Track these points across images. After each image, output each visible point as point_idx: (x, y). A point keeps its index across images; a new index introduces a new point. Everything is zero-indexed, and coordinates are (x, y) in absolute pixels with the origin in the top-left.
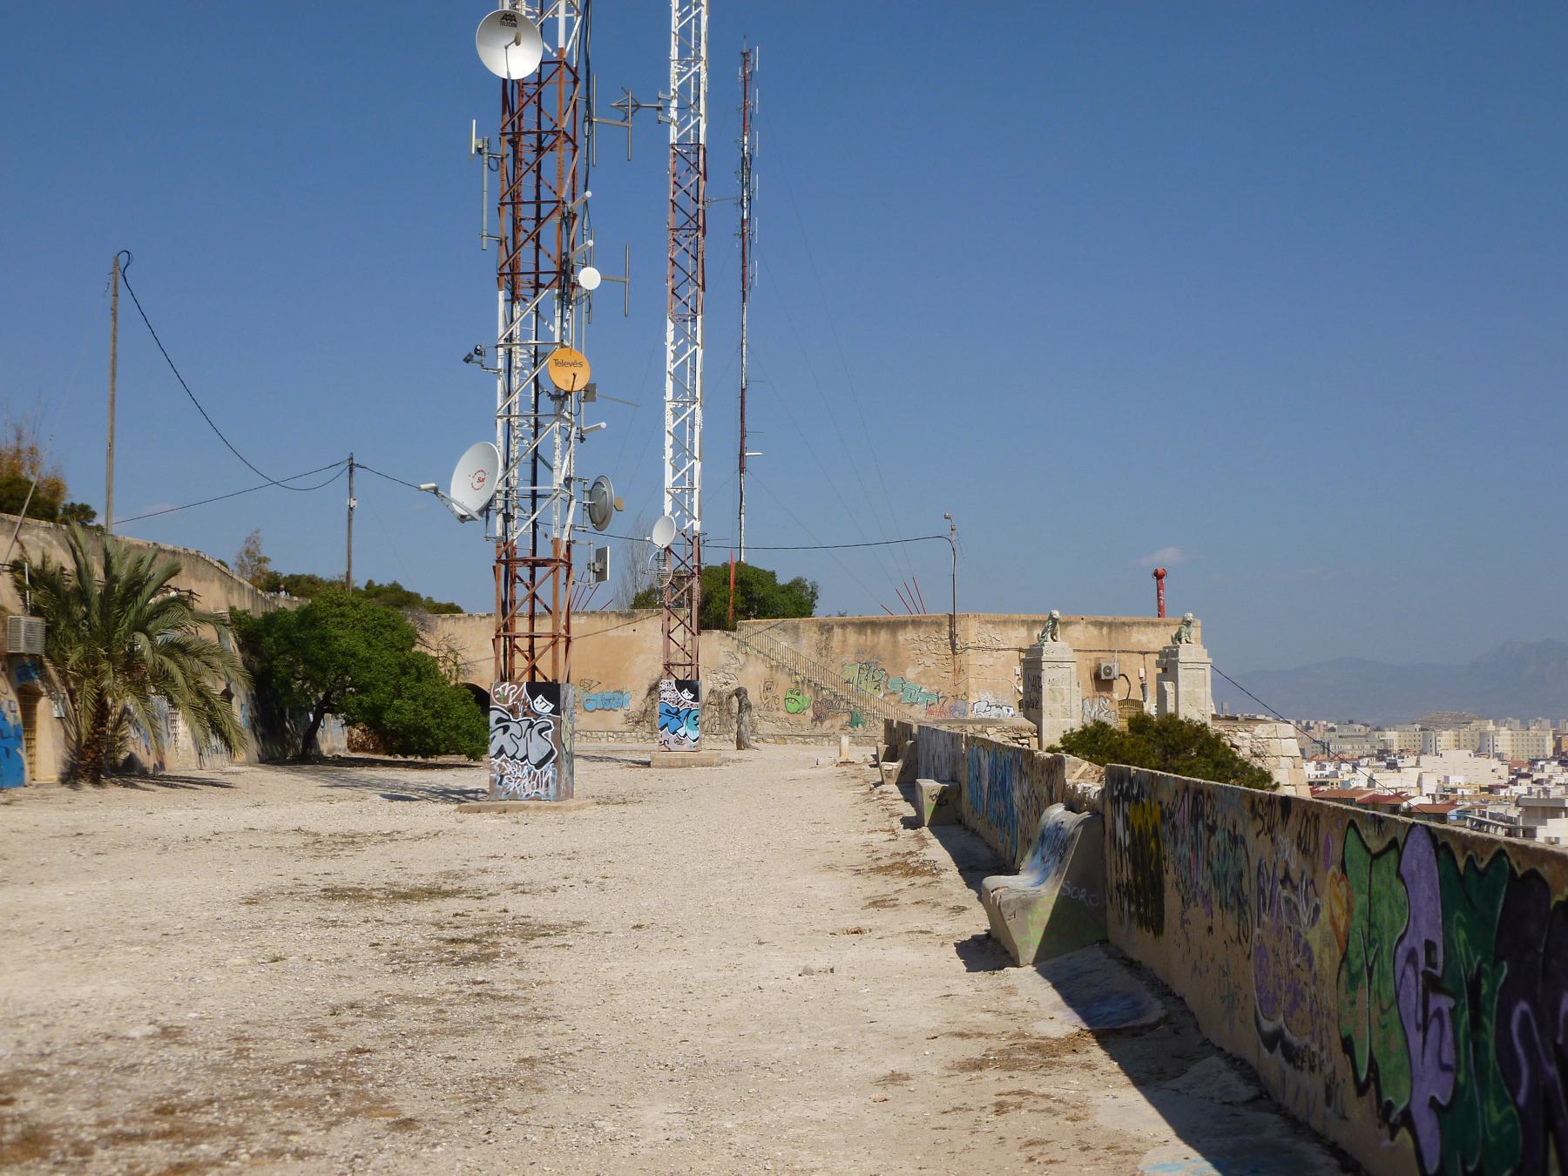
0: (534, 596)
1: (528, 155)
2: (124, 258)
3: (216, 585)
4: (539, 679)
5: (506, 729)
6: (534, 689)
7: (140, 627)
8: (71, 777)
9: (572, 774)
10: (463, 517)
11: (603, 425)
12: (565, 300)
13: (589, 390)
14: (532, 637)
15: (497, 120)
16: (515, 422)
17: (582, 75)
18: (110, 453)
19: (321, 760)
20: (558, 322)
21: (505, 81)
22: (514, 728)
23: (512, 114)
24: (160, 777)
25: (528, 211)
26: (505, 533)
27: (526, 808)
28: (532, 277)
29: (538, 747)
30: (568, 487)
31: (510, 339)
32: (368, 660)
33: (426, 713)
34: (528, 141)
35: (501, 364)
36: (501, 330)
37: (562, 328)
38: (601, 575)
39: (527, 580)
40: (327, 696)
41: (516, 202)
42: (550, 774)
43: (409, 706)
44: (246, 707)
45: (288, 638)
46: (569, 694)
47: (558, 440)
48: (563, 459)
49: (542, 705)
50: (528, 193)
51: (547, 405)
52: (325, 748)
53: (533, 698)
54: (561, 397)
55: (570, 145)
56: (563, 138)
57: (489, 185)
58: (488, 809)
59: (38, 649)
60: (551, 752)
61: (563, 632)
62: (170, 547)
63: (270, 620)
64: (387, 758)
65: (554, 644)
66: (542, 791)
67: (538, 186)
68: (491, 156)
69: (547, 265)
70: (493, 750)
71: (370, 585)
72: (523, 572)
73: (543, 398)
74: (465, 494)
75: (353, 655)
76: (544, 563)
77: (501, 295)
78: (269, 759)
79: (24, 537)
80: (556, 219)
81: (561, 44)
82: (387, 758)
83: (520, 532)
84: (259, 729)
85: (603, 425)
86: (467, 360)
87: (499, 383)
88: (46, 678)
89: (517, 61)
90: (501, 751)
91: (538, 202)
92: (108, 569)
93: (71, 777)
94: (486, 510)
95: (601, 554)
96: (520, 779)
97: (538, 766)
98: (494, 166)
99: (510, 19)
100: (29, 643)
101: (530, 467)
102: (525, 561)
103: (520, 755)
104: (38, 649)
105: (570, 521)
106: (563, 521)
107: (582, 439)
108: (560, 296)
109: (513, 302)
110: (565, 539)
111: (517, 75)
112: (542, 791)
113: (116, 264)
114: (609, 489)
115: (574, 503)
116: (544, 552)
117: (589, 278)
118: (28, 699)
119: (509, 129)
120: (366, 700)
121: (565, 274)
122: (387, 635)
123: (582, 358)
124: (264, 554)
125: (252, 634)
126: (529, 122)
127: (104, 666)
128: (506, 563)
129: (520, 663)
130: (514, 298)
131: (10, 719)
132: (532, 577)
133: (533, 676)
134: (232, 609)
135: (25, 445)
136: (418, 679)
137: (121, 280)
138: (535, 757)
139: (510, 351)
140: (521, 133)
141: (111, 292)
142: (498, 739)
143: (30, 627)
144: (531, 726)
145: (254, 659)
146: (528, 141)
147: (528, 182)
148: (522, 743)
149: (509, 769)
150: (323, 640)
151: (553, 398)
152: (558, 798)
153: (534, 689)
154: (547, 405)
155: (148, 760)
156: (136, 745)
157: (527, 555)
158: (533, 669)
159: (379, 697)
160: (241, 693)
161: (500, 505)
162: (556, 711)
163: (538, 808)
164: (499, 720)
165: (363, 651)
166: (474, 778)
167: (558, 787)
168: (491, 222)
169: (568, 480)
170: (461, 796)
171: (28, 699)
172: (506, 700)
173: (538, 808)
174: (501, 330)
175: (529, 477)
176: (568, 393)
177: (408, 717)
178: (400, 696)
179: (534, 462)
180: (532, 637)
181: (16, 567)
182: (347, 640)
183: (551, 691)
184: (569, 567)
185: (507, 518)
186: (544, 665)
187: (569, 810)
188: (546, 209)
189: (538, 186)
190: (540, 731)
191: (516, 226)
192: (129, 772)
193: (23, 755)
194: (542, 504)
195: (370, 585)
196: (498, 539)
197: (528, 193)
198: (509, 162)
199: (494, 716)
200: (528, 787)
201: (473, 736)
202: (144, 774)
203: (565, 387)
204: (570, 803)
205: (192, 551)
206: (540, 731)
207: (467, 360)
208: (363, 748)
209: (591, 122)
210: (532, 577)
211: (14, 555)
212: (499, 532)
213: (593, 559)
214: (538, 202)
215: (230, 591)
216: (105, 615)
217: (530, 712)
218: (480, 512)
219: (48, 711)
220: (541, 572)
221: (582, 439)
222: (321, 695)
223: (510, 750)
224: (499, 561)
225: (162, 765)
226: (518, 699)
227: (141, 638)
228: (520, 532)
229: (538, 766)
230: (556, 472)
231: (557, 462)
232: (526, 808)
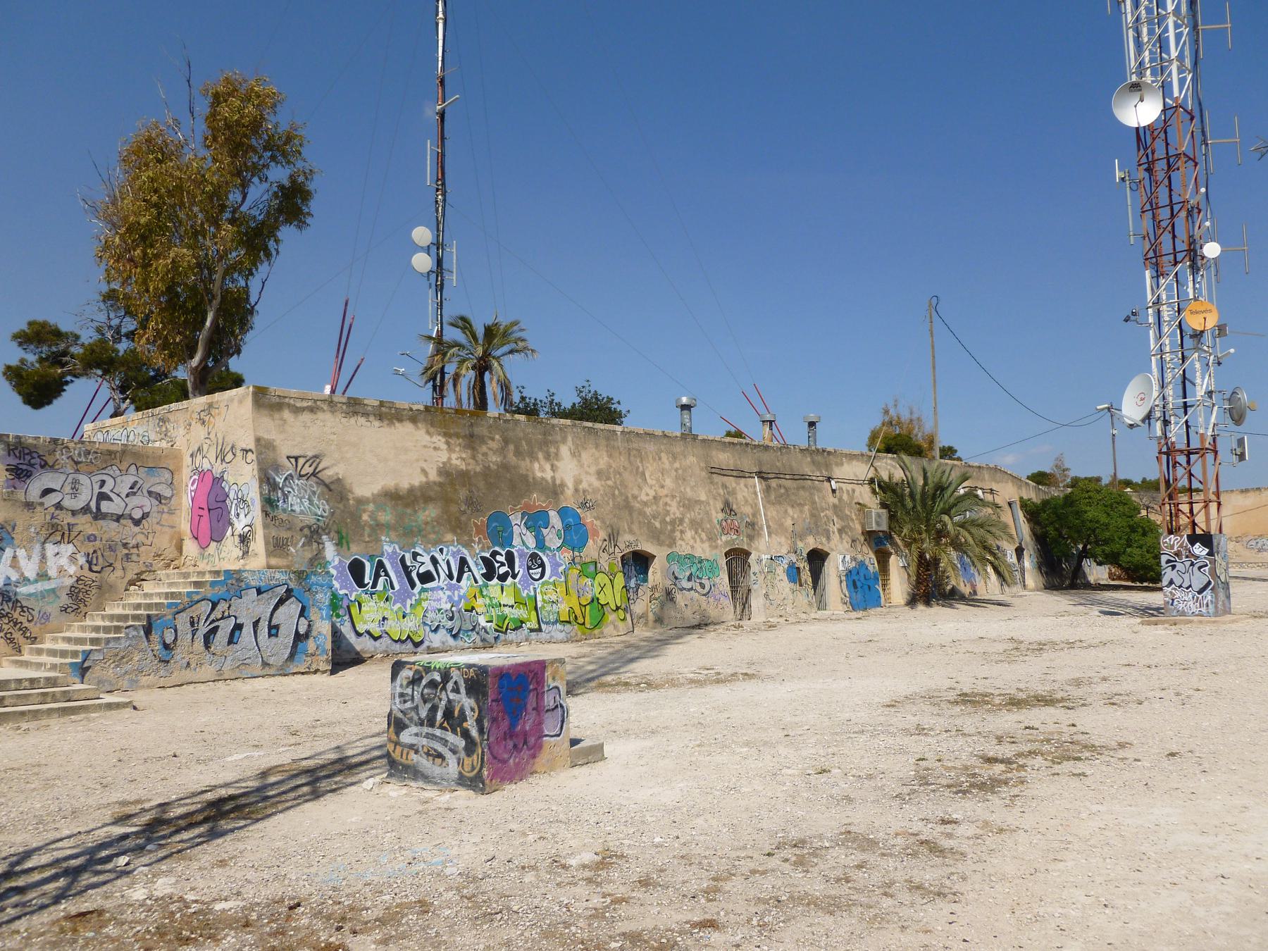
0: (1191, 475)
1: (1160, 175)
2: (934, 301)
3: (1010, 484)
4: (1198, 531)
5: (1174, 567)
6: (1193, 539)
7: (946, 511)
8: (912, 602)
9: (1228, 597)
10: (1131, 426)
11: (1232, 351)
12: (1195, 269)
13: (1221, 329)
14: (1191, 503)
15: (1133, 154)
16: (1167, 357)
17: (1196, 113)
18: (935, 414)
19: (1088, 586)
20: (1191, 284)
21: (1137, 129)
22: (1179, 566)
23: (1146, 149)
24: (972, 600)
25: (1164, 214)
26: (1165, 434)
27: (1191, 622)
28: (1172, 257)
29: (1199, 579)
30: (1211, 397)
31: (1158, 302)
32: (1107, 525)
33: (1148, 556)
34: (1161, 166)
35: (1151, 320)
36: (1149, 296)
37: (1194, 288)
38: (1242, 457)
39: (1184, 464)
40: (1085, 547)
41: (1154, 208)
42: (1209, 598)
43: (1137, 551)
44: (1034, 555)
45: (1055, 513)
46: (1223, 543)
47: (1198, 365)
48: (1203, 379)
49: (1199, 549)
50: (1163, 199)
51: (1189, 342)
52: (1091, 579)
53: (1193, 545)
54: (1198, 335)
55: (1191, 163)
56: (1183, 159)
57: (1131, 201)
58: (1163, 623)
59: (885, 527)
60: (1209, 583)
61: (1213, 497)
62: (976, 464)
63: (1045, 503)
64: (1130, 584)
65: (1206, 507)
66: (1204, 610)
67: (1170, 196)
68: (1132, 181)
69: (1182, 246)
70: (1165, 582)
71: (1144, 481)
72: (1182, 459)
73: (1186, 338)
74: (1132, 410)
75: (1097, 522)
76: (1201, 451)
77: (1148, 274)
78: (1051, 586)
79: (877, 464)
80: (1183, 214)
81: (1176, 94)
82: (1130, 584)
83: (1176, 432)
84: (1044, 569)
85: (1232, 351)
86: (1126, 320)
87: (1151, 332)
88: (894, 544)
89: (1142, 112)
90: (1171, 582)
91: (1171, 205)
92: (925, 478)
93: (912, 602)
94: (1148, 417)
95: (1241, 442)
96: (1186, 601)
97: (1200, 592)
98: (1134, 187)
99: (1136, 87)
100: (878, 524)
101: (1181, 387)
102: (1181, 451)
103: (1185, 585)
104: (885, 527)
105: (1213, 420)
106: (1208, 422)
107: (1219, 364)
108: (1192, 267)
109: (1158, 277)
110: (1210, 433)
111: (1144, 123)
112: (1204, 610)
113: (931, 304)
114: (1244, 397)
115: (1216, 408)
116: (1195, 444)
117: (1211, 250)
118: (883, 558)
119: (1144, 160)
120: (1107, 549)
121: (1193, 254)
122: (1121, 508)
123: (1214, 308)
124: (1066, 466)
125: (1033, 513)
126: (1161, 153)
127: (924, 535)
128: (1167, 454)
129: (1183, 520)
130: (1159, 274)
131: (871, 568)
132: (1188, 462)
133: (1194, 530)
134: (1021, 498)
135: (915, 416)
136: (1144, 534)
137: (934, 313)
138: (1197, 586)
139: (1159, 311)
140: (1154, 161)
141: (928, 319)
142: (1168, 574)
143: (879, 515)
144: (1192, 564)
145: (1038, 528)
146: (1161, 166)
147: (1163, 193)
148: (1186, 576)
149: (1178, 594)
150: (1078, 514)
151: (1191, 337)
152: (1216, 614)
153: (1193, 539)
154: (1189, 342)
155: (966, 590)
156: (956, 581)
157: (1184, 447)
158: (1194, 524)
159: (1116, 547)
160: (1030, 548)
161: (1158, 414)
162: (1211, 554)
163: (1201, 622)
164: (1168, 561)
165: (1103, 519)
166: (1155, 599)
167: (1216, 607)
168: (1135, 225)
169: (1210, 393)
170: (1148, 612)
171: (883, 558)
172: (1172, 547)
173: (1201, 622)
174: (1149, 296)
175: (1181, 393)
176: (1202, 332)
177: (1137, 558)
178: (1130, 546)
179: (1184, 383)
180: (1191, 503)
181: (872, 481)
182: (1092, 513)
183: (1206, 540)
184: (1216, 453)
185: (1166, 423)
186: (1200, 519)
187: (1224, 623)
188: (1176, 208)
189: (1170, 196)
190: (1200, 568)
191: (1157, 223)
192: (951, 597)
193: (880, 589)
194: (1190, 411)
195: (1144, 481)
196: (1160, 438)
197: (1163, 199)
198: (1147, 182)
199: (1164, 559)
200: (1193, 607)
201: (1150, 568)
202: (962, 598)
203: (1200, 328)
204: (1228, 617)
205: (992, 465)
206: (1200, 568)
207: (1126, 320)
208: (1119, 578)
209: (1207, 145)
210: (1188, 462)
211: (870, 475)
212: (1159, 433)
213: (1235, 445)
214: (1171, 205)
215: (1020, 487)
216: (924, 505)
217: (1190, 554)
218: (1143, 421)
219: (895, 563)
220: (1193, 457)
221: (1219, 364)
222: (1080, 546)
223: (1178, 581)
224: (1160, 452)
225: (975, 593)
226: (1181, 546)
227: (946, 518)
228: (1176, 432)
229: (1200, 592)
230: (1198, 388)
231: (1198, 381)
232: (1191, 622)
